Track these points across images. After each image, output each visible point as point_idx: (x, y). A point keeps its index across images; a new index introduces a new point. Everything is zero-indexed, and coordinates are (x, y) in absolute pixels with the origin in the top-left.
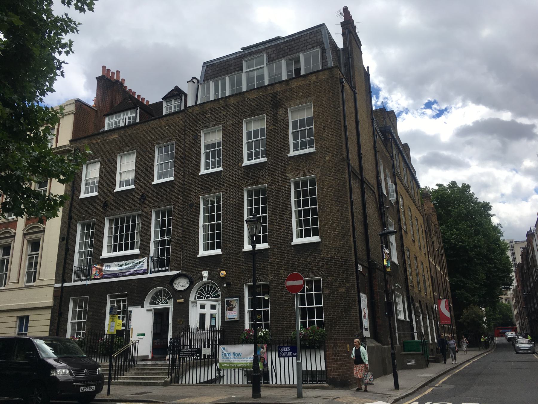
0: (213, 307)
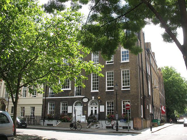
0: (96, 108)
